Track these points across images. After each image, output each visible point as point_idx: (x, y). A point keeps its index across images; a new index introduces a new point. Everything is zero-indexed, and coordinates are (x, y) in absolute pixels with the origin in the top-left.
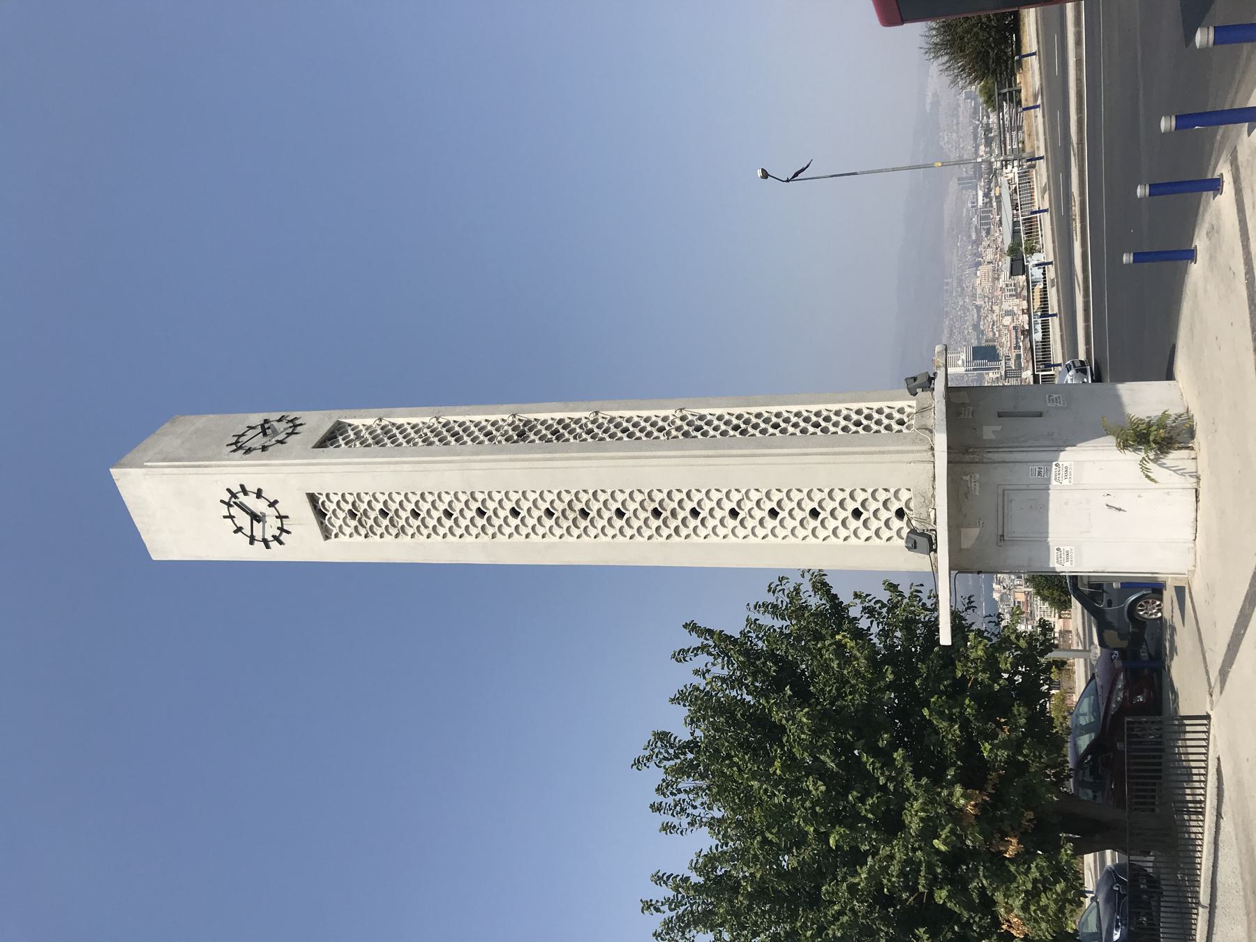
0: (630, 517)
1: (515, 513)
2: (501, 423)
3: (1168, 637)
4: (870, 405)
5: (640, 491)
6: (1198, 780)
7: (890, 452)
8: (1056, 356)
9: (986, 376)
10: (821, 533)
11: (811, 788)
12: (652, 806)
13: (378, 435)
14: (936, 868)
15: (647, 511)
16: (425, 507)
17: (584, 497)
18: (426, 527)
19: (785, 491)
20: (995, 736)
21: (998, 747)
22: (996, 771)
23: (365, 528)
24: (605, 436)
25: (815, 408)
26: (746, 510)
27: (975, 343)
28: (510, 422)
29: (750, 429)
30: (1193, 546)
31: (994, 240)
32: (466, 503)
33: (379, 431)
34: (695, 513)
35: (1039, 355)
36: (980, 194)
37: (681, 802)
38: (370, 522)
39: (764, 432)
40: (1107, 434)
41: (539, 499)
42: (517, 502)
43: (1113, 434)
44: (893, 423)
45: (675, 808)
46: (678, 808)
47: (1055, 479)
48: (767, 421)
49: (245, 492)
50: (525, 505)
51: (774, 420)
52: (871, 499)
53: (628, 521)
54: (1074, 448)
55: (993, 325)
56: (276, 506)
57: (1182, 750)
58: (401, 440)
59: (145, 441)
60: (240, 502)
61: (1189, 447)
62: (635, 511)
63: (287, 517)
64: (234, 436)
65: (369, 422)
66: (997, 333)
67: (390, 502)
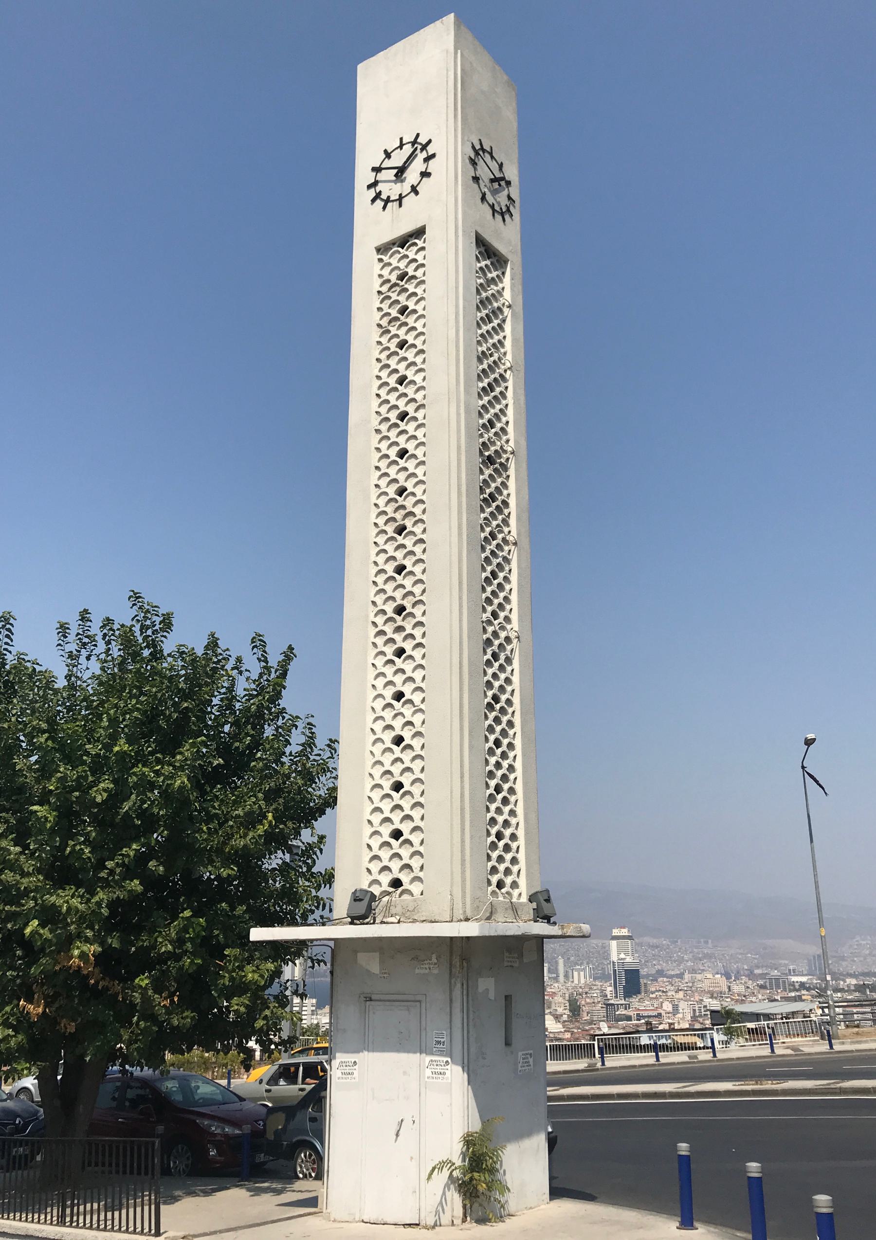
0: (396, 581)
1: (403, 453)
2: (504, 438)
3: (274, 1186)
4: (522, 850)
5: (424, 591)
6: (108, 1218)
7: (463, 872)
8: (613, 1060)
9: (608, 984)
10: (376, 795)
11: (102, 785)
12: (86, 611)
13: (491, 303)
14: (13, 923)
15: (403, 599)
16: (410, 354)
17: (418, 529)
18: (388, 357)
19: (422, 753)
20: (158, 990)
21: (144, 995)
22: (123, 989)
23: (389, 291)
24: (488, 553)
25: (519, 787)
26: (402, 710)
27: (643, 972)
28: (505, 448)
29: (494, 714)
30: (357, 1219)
31: (754, 993)
32: (413, 400)
33: (495, 305)
34: (400, 652)
35: (623, 1041)
36: (804, 979)
37: (93, 643)
38: (394, 296)
39: (491, 729)
40: (483, 1122)
41: (416, 480)
42: (414, 456)
43: (484, 1129)
44: (500, 876)
45: (85, 637)
46: (86, 640)
47: (432, 1061)
48: (504, 733)
49: (427, 160)
50: (411, 465)
51: (505, 742)
52: (412, 850)
53: (392, 578)
54: (466, 1083)
55: (663, 992)
56: (412, 194)
57: (139, 1200)
58: (485, 328)
59: (486, 52)
60: (417, 155)
61: (466, 1217)
62: (403, 586)
63: (400, 205)
64: (491, 148)
65: (507, 295)
66: (654, 996)
67: (415, 316)
